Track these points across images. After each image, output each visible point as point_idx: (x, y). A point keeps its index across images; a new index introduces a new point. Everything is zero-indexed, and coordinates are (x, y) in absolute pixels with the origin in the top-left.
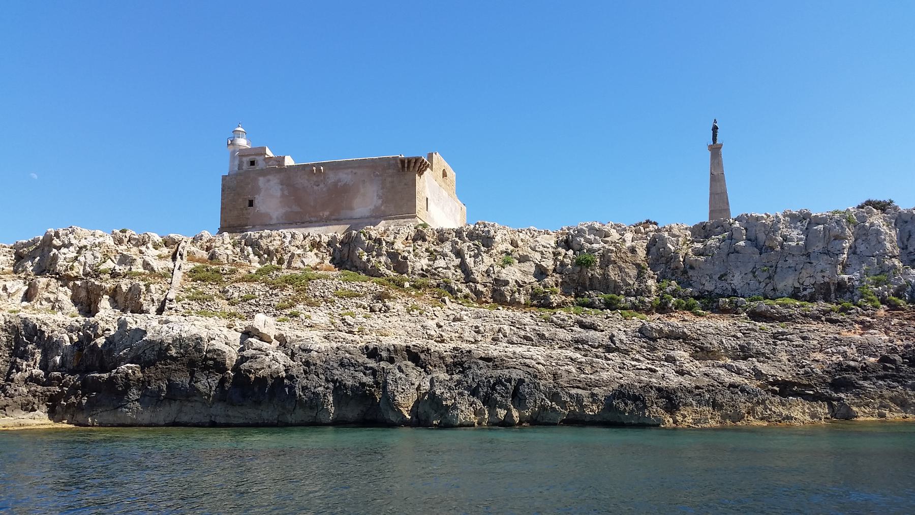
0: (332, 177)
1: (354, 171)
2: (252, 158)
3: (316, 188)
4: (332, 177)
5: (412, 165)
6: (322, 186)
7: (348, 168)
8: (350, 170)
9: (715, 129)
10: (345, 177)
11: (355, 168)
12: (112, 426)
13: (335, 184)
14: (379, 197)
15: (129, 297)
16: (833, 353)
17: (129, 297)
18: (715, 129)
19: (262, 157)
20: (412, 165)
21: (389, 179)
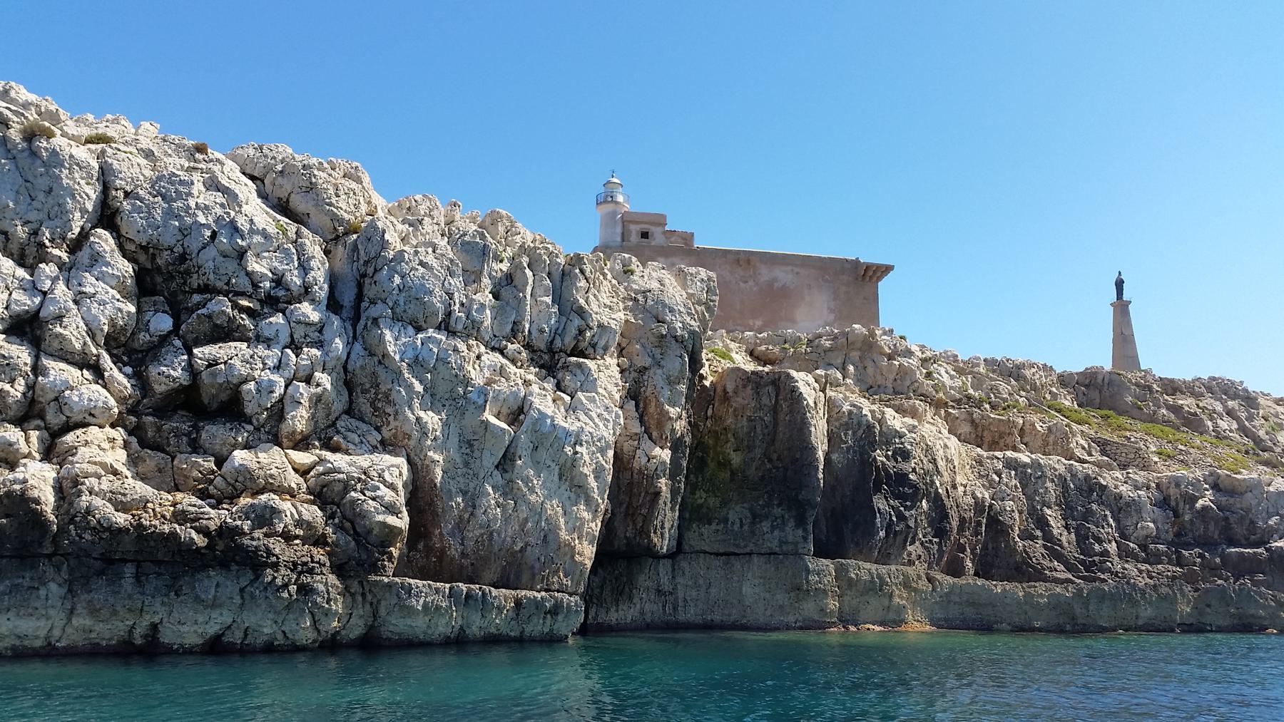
0: (765, 274)
1: (796, 270)
2: (645, 227)
3: (742, 285)
4: (765, 274)
5: (871, 273)
6: (751, 283)
7: (787, 264)
8: (790, 268)
9: (1119, 284)
10: (784, 276)
11: (796, 266)
12: (1158, 630)
13: (770, 284)
14: (831, 311)
15: (1051, 439)
16: (1068, 684)
17: (1051, 439)
18: (1119, 284)
19: (659, 229)
20: (871, 273)
21: (844, 288)
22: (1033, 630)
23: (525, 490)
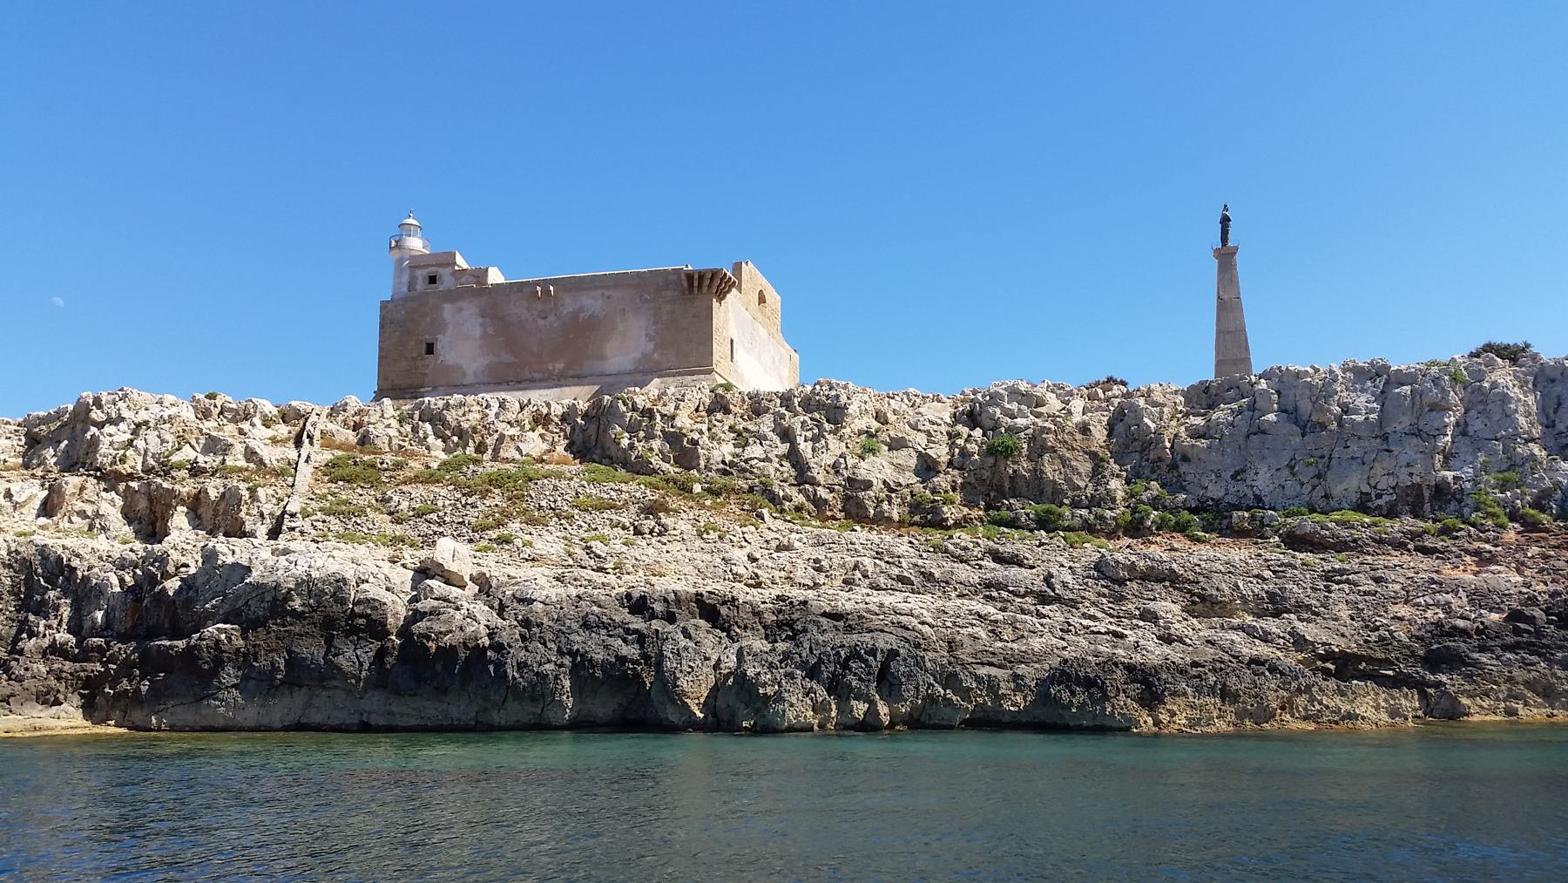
0: (569, 304)
1: (607, 293)
2: (431, 270)
3: (541, 322)
4: (569, 304)
5: (707, 282)
6: (551, 318)
7: (597, 288)
8: (599, 292)
9: (1225, 221)
10: (591, 303)
11: (608, 288)
12: (192, 730)
13: (575, 316)
14: (650, 338)
15: (221, 509)
17: (221, 509)
18: (1225, 221)
19: (449, 270)
20: (707, 282)
21: (667, 307)
22: (952, 728)
23: (1488, 547)
